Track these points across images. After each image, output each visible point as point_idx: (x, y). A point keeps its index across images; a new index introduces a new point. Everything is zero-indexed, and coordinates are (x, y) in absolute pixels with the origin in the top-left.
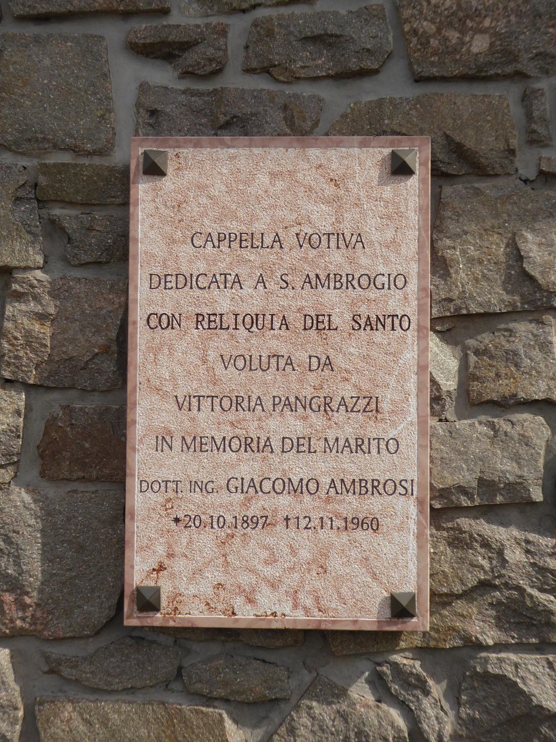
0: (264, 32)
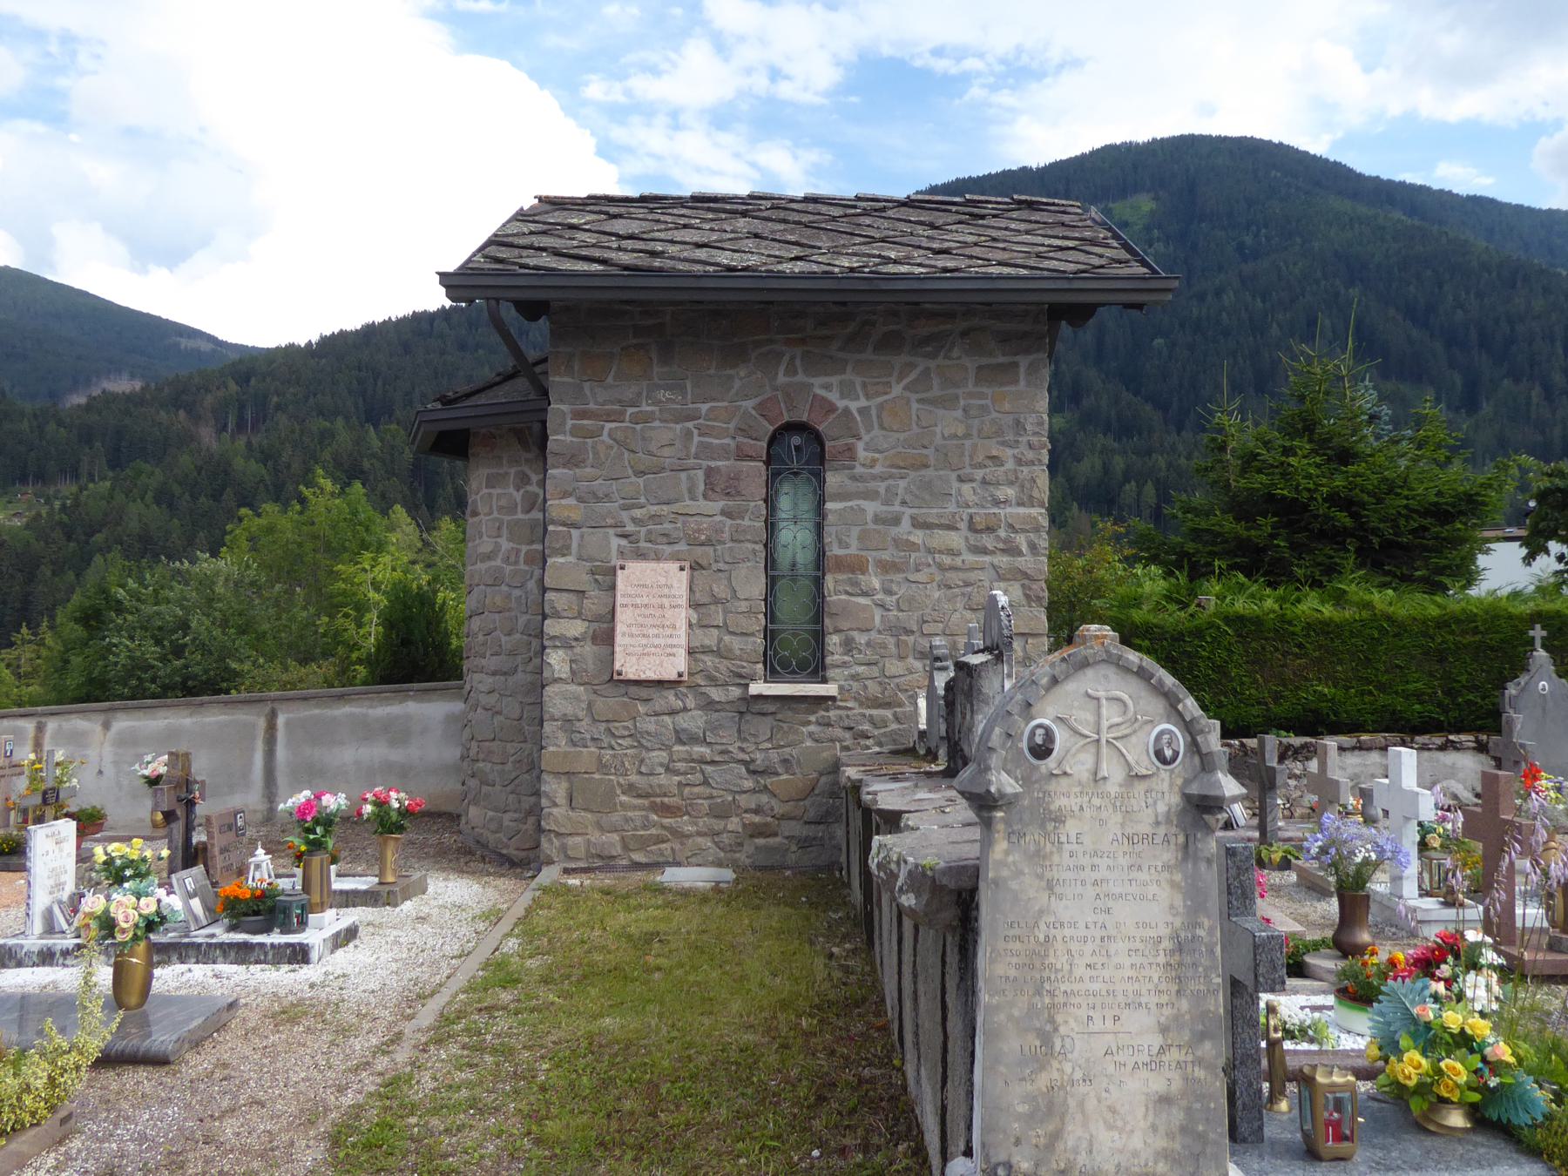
0: (650, 532)
